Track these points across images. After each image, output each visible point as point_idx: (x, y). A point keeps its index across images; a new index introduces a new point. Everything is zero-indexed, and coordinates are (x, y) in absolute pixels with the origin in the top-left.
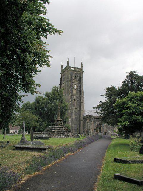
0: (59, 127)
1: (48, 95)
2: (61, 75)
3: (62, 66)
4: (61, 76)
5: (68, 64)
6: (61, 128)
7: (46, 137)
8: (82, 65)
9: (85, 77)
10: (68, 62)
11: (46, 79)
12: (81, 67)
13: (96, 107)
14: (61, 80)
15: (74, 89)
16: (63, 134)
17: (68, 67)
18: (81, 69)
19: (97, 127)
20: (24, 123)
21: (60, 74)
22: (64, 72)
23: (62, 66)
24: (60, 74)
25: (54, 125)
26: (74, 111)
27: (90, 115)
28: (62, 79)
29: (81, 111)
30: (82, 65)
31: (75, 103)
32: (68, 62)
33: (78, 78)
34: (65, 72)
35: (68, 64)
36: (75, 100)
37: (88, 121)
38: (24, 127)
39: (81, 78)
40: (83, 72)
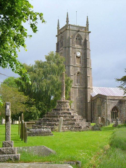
0: (65, 113)
1: (40, 65)
2: (58, 38)
3: (58, 25)
4: (58, 40)
5: (67, 21)
6: (67, 115)
7: (47, 132)
8: (87, 22)
9: (92, 39)
10: (67, 19)
11: (36, 47)
12: (86, 26)
13: (120, 78)
14: (58, 44)
15: (77, 57)
16: (71, 124)
17: (67, 25)
18: (87, 28)
19: (112, 112)
20: (8, 107)
21: (57, 36)
22: (61, 33)
23: (58, 25)
24: (57, 36)
25: (55, 109)
26: (77, 89)
27: (101, 95)
28: (60, 43)
29: (88, 90)
30: (87, 22)
31: (79, 76)
32: (67, 19)
33: (83, 41)
34: (63, 33)
35: (67, 21)
36: (78, 73)
37: (98, 103)
38: (8, 116)
39: (87, 42)
40: (90, 32)
